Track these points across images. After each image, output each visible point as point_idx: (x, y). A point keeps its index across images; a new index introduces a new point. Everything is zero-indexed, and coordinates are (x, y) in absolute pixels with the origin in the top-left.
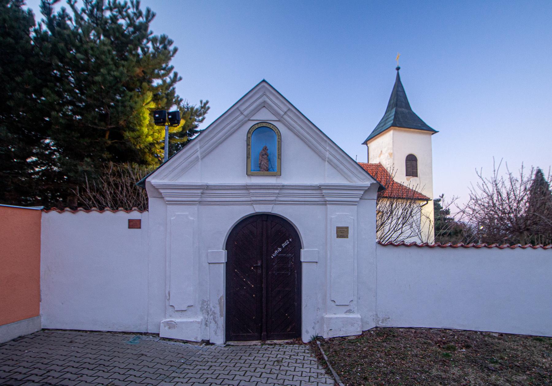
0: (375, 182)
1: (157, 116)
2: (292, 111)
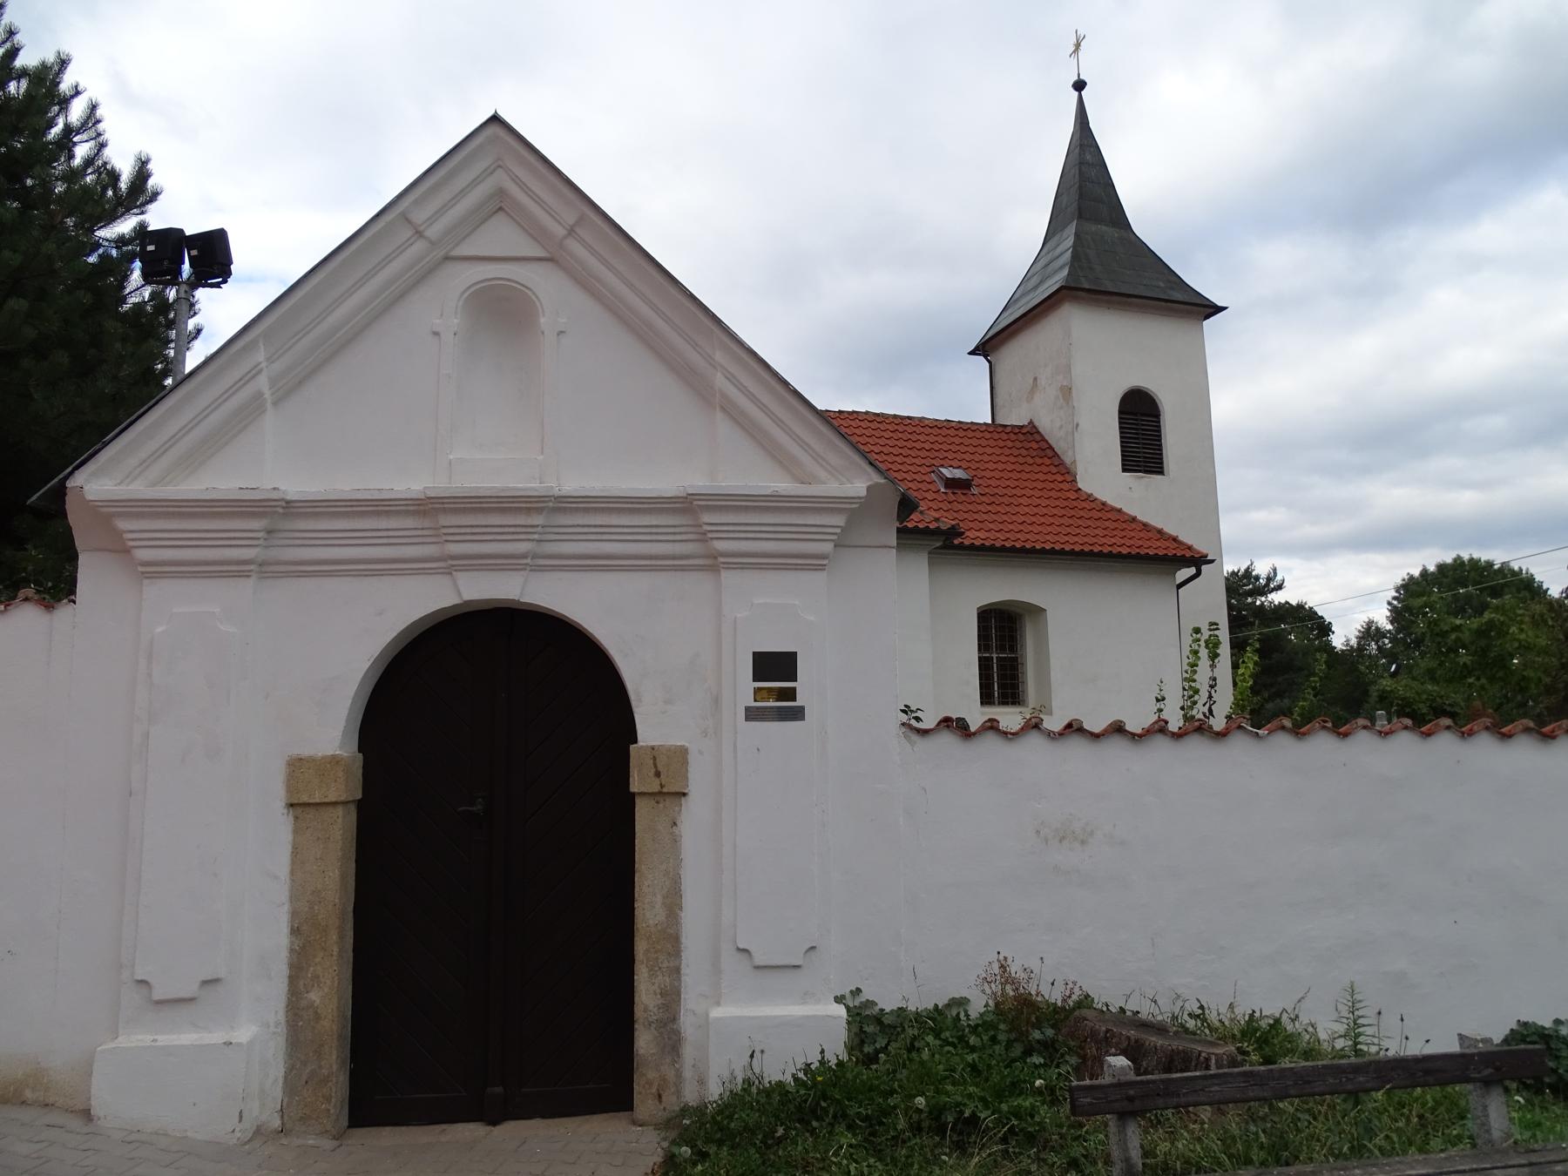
1: (151, 248)
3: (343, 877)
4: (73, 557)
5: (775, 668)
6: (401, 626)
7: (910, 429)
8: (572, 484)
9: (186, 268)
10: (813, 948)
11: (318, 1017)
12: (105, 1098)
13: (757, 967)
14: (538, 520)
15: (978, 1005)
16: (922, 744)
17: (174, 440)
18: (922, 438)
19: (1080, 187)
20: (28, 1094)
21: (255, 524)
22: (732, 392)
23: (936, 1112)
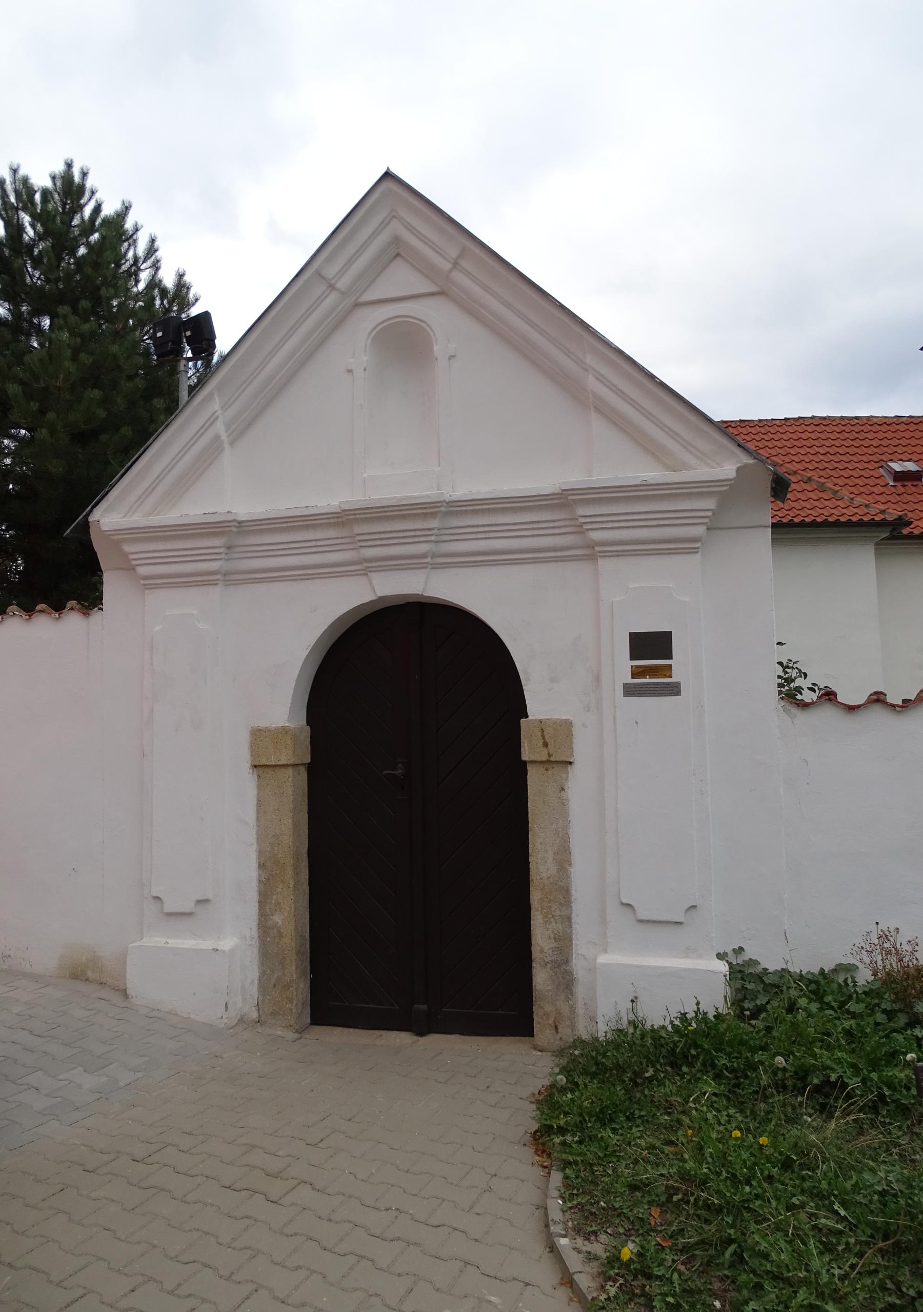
0: (752, 461)
3: (296, 825)
5: (651, 646)
6: (330, 621)
7: (857, 429)
8: (465, 488)
10: (694, 907)
11: (281, 936)
12: (134, 982)
13: (641, 921)
14: (434, 523)
15: (864, 977)
16: (802, 716)
17: (159, 479)
18: (870, 436)
20: (90, 974)
21: (217, 542)
22: (603, 391)
23: (802, 1074)
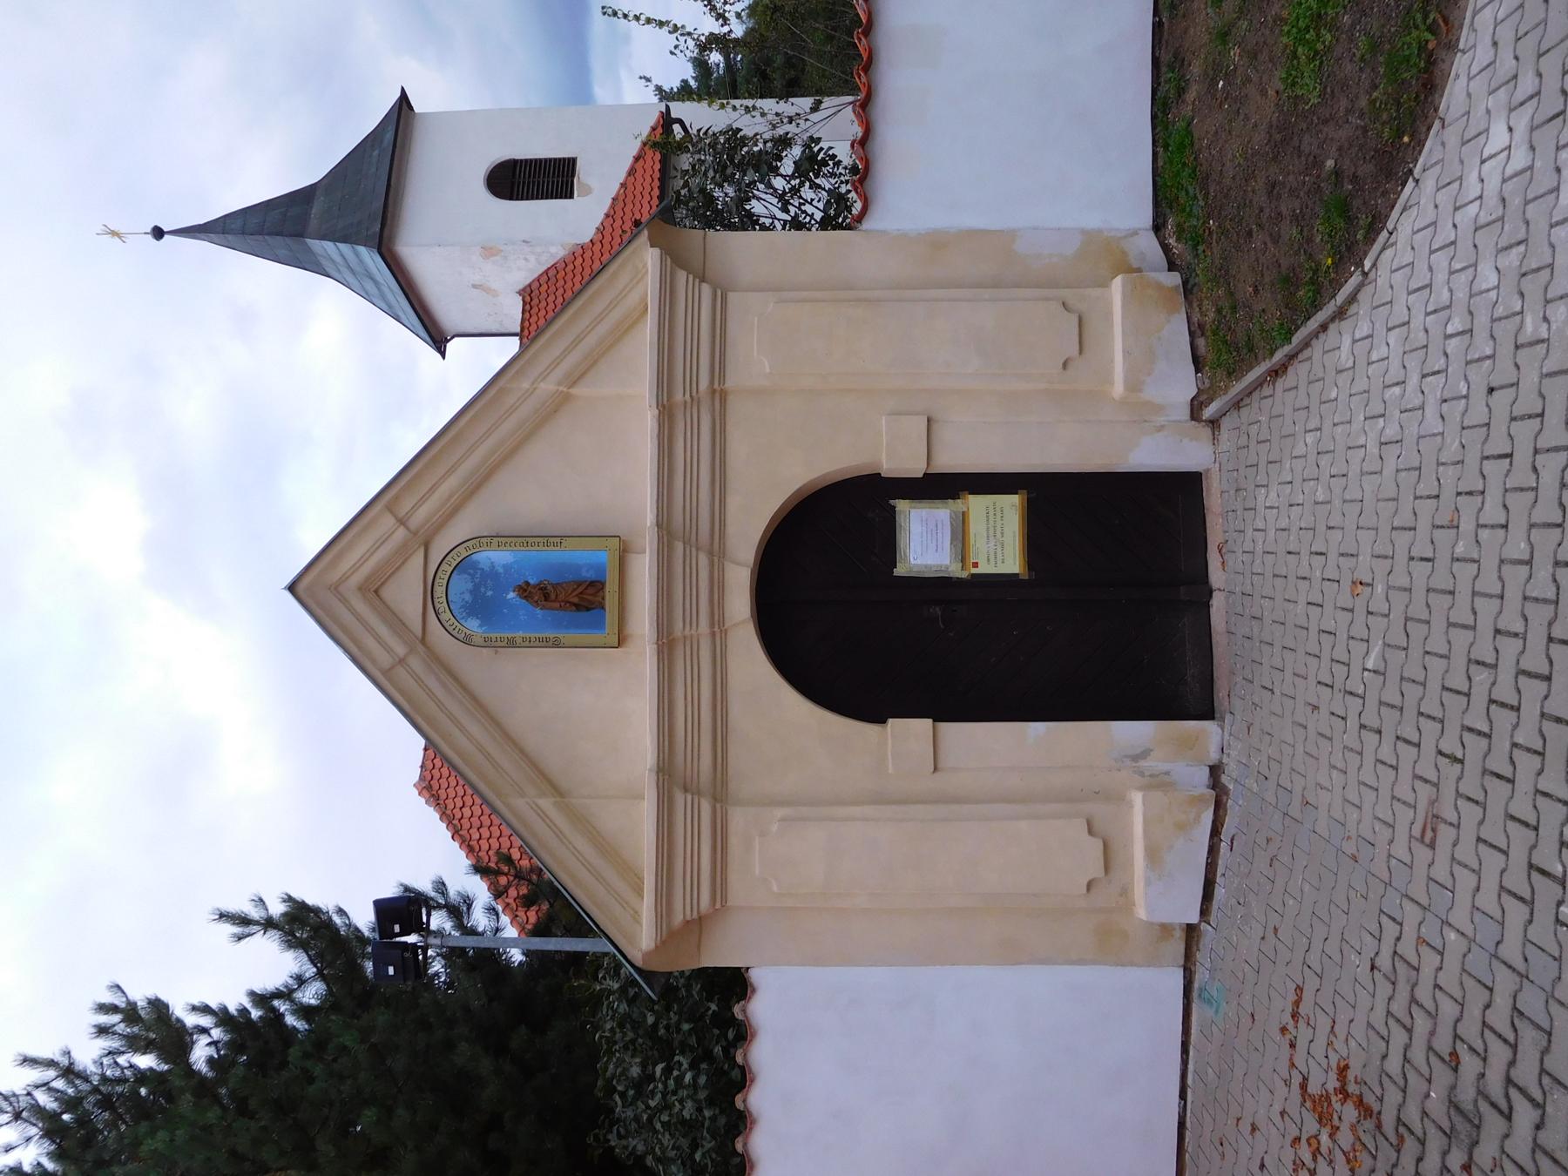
2: (397, 498)
4: (703, 971)
9: (412, 939)
19: (270, 234)
